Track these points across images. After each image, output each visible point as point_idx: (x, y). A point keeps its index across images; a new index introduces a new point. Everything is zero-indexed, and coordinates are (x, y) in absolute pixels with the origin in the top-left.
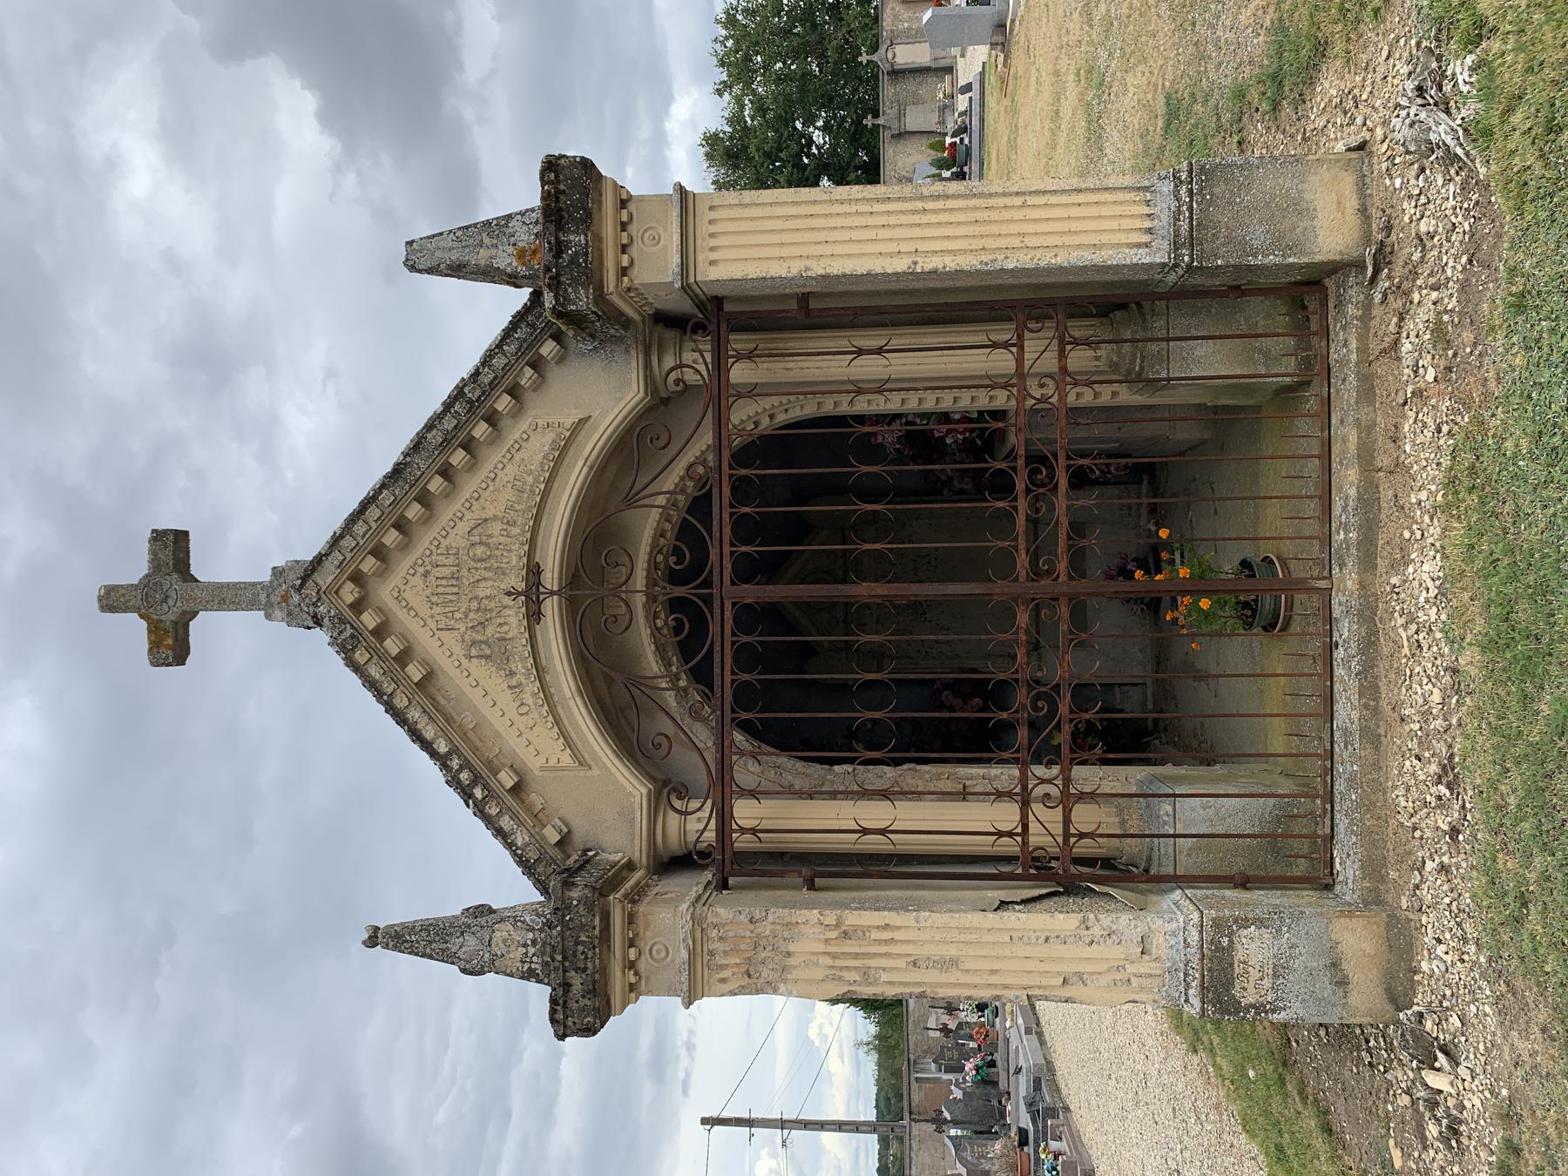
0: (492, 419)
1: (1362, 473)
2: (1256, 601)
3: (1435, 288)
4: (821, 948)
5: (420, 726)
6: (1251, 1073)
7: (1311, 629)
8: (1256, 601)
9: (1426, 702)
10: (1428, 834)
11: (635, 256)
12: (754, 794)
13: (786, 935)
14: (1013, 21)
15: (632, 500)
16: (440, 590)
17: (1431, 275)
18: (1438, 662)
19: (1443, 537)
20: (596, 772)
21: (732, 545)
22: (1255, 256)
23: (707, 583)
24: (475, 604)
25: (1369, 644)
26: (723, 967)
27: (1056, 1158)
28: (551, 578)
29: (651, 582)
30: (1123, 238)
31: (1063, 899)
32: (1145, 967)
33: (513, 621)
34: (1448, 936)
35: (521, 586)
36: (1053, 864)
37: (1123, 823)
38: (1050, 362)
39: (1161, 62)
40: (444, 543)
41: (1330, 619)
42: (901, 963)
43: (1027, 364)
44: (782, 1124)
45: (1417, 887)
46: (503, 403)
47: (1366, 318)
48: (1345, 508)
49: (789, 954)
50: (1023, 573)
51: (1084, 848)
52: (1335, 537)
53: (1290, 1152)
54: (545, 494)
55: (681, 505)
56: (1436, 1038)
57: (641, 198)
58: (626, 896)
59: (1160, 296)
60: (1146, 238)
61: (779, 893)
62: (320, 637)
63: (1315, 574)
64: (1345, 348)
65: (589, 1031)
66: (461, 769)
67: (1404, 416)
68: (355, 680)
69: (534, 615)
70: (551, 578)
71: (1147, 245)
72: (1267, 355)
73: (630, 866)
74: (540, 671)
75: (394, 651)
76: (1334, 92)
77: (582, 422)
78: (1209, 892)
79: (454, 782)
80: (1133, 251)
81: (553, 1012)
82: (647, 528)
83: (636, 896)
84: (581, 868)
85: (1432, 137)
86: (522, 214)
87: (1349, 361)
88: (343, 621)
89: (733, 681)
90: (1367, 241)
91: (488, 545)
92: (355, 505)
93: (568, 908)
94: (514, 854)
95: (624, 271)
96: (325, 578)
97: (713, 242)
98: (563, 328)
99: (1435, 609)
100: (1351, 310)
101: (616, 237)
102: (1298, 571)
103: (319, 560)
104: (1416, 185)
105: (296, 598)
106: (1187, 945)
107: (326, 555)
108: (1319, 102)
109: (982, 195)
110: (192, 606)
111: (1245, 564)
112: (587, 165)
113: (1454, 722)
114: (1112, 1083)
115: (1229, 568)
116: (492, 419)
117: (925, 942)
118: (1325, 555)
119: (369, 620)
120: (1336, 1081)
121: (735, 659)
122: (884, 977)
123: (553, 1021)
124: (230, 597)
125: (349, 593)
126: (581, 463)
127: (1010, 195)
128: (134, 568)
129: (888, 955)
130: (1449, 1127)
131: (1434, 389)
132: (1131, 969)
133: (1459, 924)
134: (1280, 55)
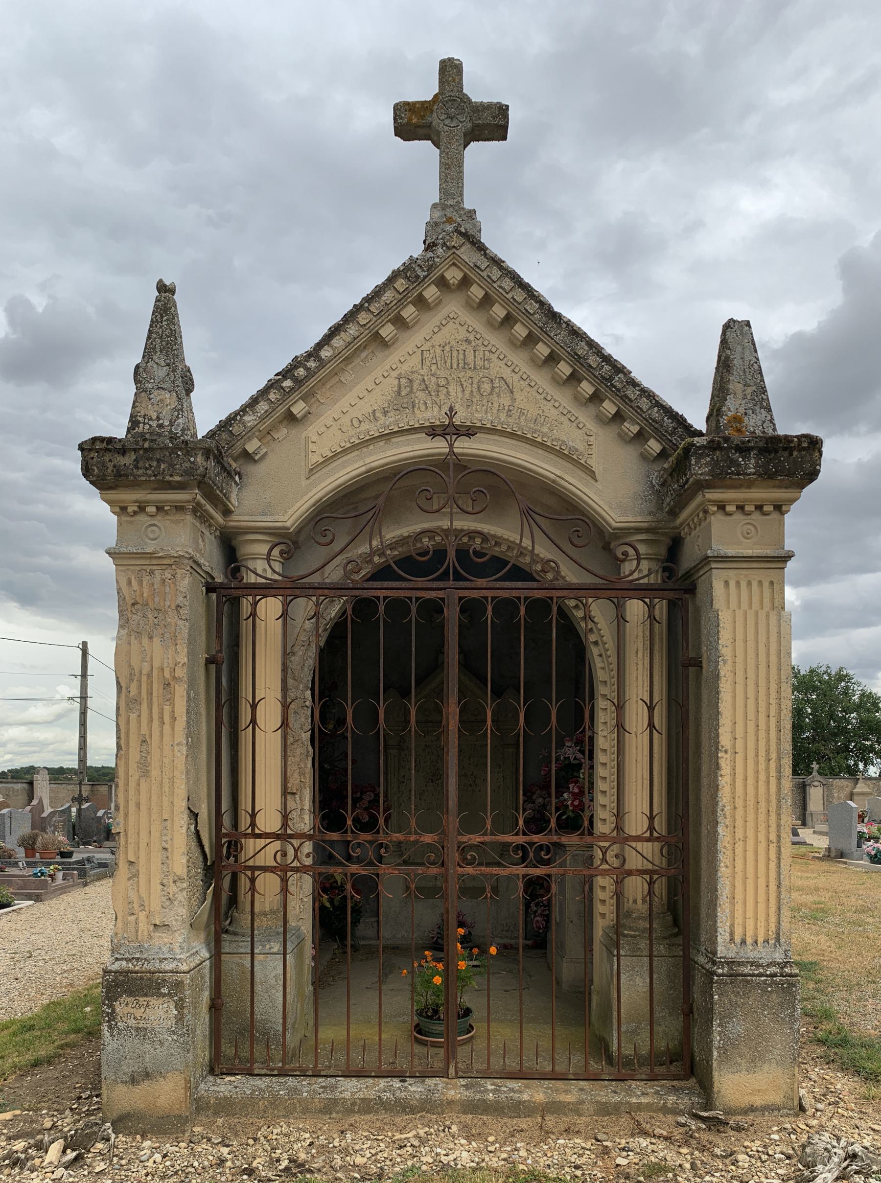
0: (596, 398)
1: (541, 1104)
2: (439, 1019)
3: (693, 1166)
4: (156, 664)
5: (342, 334)
6: (88, 1009)
7: (416, 1061)
8: (439, 1019)
9: (356, 1152)
10: (251, 1150)
11: (734, 517)
12: (284, 615)
13: (167, 635)
14: (845, 863)
15: (528, 514)
16: (455, 354)
17: (703, 1162)
18: (388, 1163)
19: (489, 1169)
20: (304, 483)
21: (493, 598)
22: (720, 1025)
23: (458, 577)
24: (443, 382)
25: (404, 1107)
26: (140, 583)
27: (50, 876)
28: (464, 446)
29: (458, 533)
30: (738, 920)
31: (202, 865)
32: (143, 926)
33: (428, 414)
34: (168, 1163)
35: (457, 421)
36: (232, 859)
37: (265, 914)
38: (634, 862)
39: (840, 959)
40: (494, 357)
41: (423, 1076)
42: (144, 730)
43: (634, 844)
44: (84, 697)
45: (209, 1140)
46: (609, 407)
47: (665, 1110)
48: (512, 1090)
49: (151, 638)
50: (464, 839)
51: (244, 882)
52: (489, 1082)
53: (27, 1036)
54: (533, 442)
55: (521, 559)
56: (89, 1151)
57: (782, 524)
58: (198, 504)
59: (686, 948)
60: (738, 939)
61: (204, 633)
62: (417, 250)
63: (459, 1065)
64: (641, 1094)
65: (87, 471)
66: (307, 369)
67: (586, 1139)
68: (381, 280)
69: (433, 432)
70: (464, 446)
71: (732, 940)
72: (635, 1032)
73: (227, 512)
74: (387, 437)
75: (405, 314)
76: (839, 1086)
77: (592, 474)
78: (207, 979)
79: (296, 363)
80: (727, 929)
81: (102, 439)
82: (505, 530)
83: (197, 510)
84: (224, 469)
85: (820, 1167)
86: (772, 421)
87: (631, 1096)
88: (430, 268)
89: (378, 598)
90: (729, 1112)
91: (491, 394)
92: (527, 279)
93: (188, 454)
94: (237, 413)
95: (722, 507)
96: (467, 254)
97: (744, 584)
98: (671, 459)
99: (431, 1161)
100: (672, 1099)
101: (750, 501)
102: (462, 1052)
103: (482, 248)
104: (777, 1152)
105: (449, 228)
106: (161, 961)
107: (485, 255)
108: (829, 1075)
109: (779, 807)
110: (444, 140)
111: (468, 1012)
112: (812, 475)
113: (339, 1175)
114: (99, 915)
115: (466, 1000)
116: (596, 398)
117: (162, 750)
118: (474, 1074)
119: (431, 292)
120: (72, 1071)
121: (397, 600)
122: (133, 716)
123: (94, 440)
124: (451, 173)
125: (453, 275)
126: (558, 472)
127: (778, 831)
128: (479, 87)
129: (151, 719)
130: (18, 1159)
131: (610, 1164)
132: (142, 916)
133: (176, 1173)
134: (863, 1046)
